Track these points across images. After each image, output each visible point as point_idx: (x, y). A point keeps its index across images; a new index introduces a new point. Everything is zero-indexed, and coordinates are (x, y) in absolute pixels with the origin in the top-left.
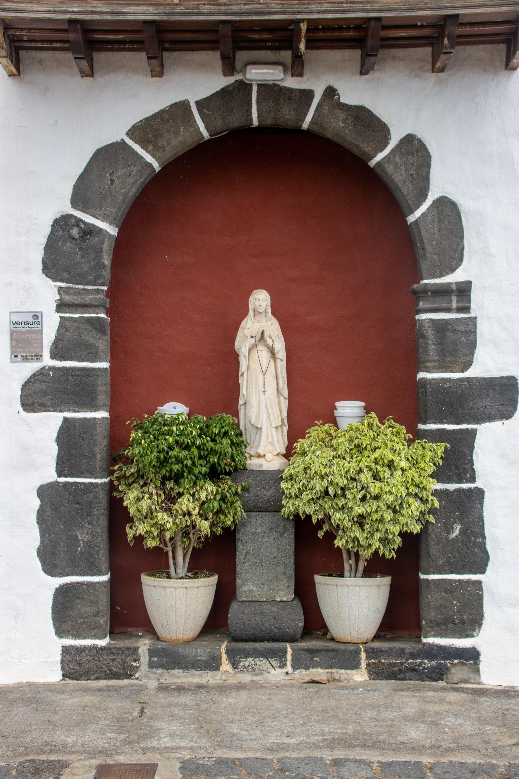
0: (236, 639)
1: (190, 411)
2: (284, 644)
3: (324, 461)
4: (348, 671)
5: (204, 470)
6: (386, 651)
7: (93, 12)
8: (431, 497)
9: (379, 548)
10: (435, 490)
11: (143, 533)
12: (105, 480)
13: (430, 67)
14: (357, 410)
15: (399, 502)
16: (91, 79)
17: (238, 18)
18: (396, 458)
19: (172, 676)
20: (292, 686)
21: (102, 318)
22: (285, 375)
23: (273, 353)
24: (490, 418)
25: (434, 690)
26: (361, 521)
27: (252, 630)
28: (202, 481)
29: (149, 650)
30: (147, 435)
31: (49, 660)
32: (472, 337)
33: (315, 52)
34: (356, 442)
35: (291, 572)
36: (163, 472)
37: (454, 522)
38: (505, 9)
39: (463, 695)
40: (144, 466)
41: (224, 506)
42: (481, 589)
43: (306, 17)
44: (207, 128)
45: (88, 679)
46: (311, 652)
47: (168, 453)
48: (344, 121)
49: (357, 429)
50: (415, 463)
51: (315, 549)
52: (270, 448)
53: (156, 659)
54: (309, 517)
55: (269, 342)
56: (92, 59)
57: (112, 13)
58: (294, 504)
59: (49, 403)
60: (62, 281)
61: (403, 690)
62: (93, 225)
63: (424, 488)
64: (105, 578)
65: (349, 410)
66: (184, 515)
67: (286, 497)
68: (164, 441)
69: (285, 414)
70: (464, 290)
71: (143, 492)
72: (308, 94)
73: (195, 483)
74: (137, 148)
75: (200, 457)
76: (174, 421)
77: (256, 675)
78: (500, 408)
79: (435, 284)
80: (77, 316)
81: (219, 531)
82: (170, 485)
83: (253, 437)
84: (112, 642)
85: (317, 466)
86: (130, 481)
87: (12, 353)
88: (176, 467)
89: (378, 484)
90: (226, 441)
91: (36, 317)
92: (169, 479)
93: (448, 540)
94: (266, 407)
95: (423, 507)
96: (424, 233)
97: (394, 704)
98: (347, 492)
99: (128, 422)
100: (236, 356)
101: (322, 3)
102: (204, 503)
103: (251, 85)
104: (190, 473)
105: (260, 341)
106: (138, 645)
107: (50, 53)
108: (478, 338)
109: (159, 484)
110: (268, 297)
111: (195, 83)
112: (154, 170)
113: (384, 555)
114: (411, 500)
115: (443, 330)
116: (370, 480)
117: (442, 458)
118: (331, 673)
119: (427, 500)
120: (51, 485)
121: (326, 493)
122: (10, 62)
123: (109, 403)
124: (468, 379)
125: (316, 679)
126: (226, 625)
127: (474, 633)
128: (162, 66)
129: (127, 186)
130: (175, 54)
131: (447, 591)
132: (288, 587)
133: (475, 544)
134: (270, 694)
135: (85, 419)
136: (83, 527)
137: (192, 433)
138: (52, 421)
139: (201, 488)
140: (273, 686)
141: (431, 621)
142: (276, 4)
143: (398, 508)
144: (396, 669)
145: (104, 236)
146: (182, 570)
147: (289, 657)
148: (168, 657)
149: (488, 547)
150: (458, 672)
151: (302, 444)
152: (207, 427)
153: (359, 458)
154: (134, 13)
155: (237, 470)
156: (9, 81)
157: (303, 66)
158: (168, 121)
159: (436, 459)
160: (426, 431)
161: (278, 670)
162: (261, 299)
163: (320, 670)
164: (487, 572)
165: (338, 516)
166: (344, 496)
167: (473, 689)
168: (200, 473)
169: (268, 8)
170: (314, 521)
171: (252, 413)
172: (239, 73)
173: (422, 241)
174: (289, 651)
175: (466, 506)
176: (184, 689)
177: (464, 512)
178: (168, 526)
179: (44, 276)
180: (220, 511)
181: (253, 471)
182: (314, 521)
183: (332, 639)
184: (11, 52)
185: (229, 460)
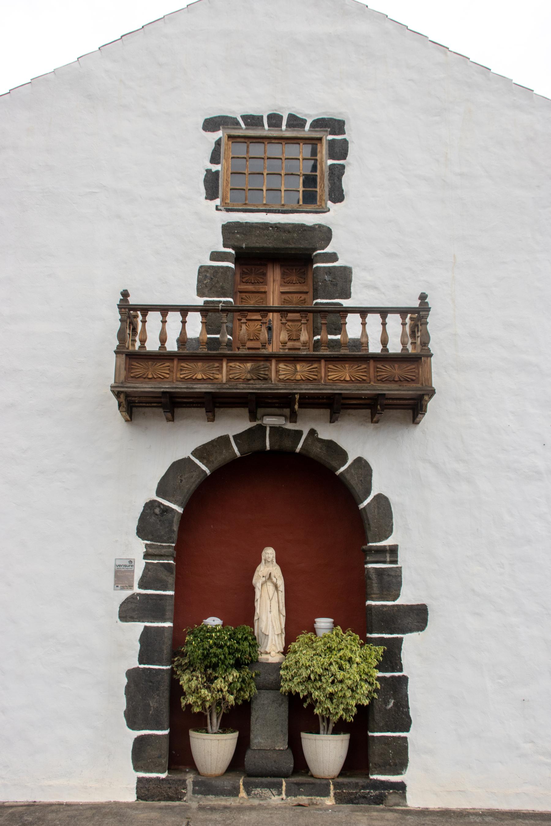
0: (249, 775)
1: (223, 623)
2: (281, 779)
3: (308, 657)
4: (322, 798)
5: (232, 662)
6: (347, 784)
8: (375, 682)
9: (343, 715)
10: (378, 677)
11: (191, 703)
12: (168, 667)
13: (370, 420)
14: (328, 624)
15: (355, 684)
16: (173, 423)
17: (259, 391)
18: (353, 656)
19: (208, 800)
20: (286, 808)
21: (171, 563)
22: (284, 601)
23: (276, 587)
24: (411, 631)
25: (377, 811)
26: (331, 696)
27: (260, 769)
28: (230, 669)
29: (193, 781)
30: (196, 639)
31: (128, 786)
32: (399, 579)
33: (304, 410)
34: (328, 645)
35: (286, 730)
36: (206, 663)
37: (390, 698)
38: (411, 392)
39: (396, 814)
40: (194, 659)
41: (244, 686)
42: (407, 743)
44: (239, 450)
45: (153, 801)
46: (298, 784)
47: (209, 650)
48: (321, 448)
49: (329, 636)
50: (365, 659)
51: (302, 716)
52: (274, 648)
53: (197, 788)
54: (298, 694)
55: (274, 580)
56: (174, 412)
57: (187, 388)
58: (288, 685)
59: (136, 617)
60: (148, 540)
61: (357, 811)
62: (168, 506)
63: (371, 676)
64: (166, 732)
65: (323, 624)
66: (218, 691)
67: (284, 681)
68: (207, 643)
69: (283, 626)
70: (393, 550)
71: (193, 676)
72: (300, 433)
73: (226, 671)
74: (197, 461)
75: (229, 654)
76: (213, 630)
77: (262, 800)
78: (417, 624)
79: (376, 546)
80: (156, 562)
81: (240, 702)
82: (209, 671)
83: (263, 641)
84: (170, 775)
85: (303, 661)
86: (184, 668)
87: (115, 585)
88: (214, 660)
89: (342, 673)
90: (246, 643)
91: (131, 562)
92: (209, 667)
93: (386, 709)
94: (272, 621)
95: (370, 688)
96: (369, 515)
97: (352, 821)
98: (322, 678)
99: (184, 630)
100: (252, 589)
102: (231, 684)
103: (266, 427)
104: (222, 664)
105: (268, 579)
106: (186, 778)
107: (150, 409)
108: (403, 580)
109: (203, 670)
111: (233, 426)
112: (206, 474)
113: (346, 719)
114: (363, 683)
115: (382, 574)
116: (337, 670)
117: (382, 656)
118: (311, 799)
119: (373, 683)
120: (136, 670)
121: (309, 678)
123: (172, 617)
124: (397, 606)
125: (301, 803)
126: (243, 765)
127: (403, 772)
128: (214, 416)
129: (190, 484)
131: (385, 744)
132: (284, 740)
133: (403, 712)
134: (271, 814)
135: (158, 627)
136: (154, 698)
137: (225, 637)
138: (138, 627)
139: (230, 674)
140: (273, 808)
141: (375, 764)
143: (354, 688)
144: (353, 796)
145: (175, 513)
146: (216, 728)
147: (284, 788)
148: (206, 787)
149: (411, 714)
150: (392, 799)
151: (294, 645)
152: (234, 633)
153: (330, 656)
154: (200, 388)
155: (253, 662)
157: (296, 418)
158: (216, 446)
159: (378, 657)
160: (371, 638)
161: (277, 797)
162: (269, 553)
163: (304, 797)
164: (410, 731)
165: (317, 693)
166: (320, 680)
167: (402, 810)
168: (229, 664)
170: (301, 696)
171: (263, 625)
173: (368, 520)
174: (284, 784)
175: (397, 688)
176: (215, 809)
177: (396, 691)
178: (208, 698)
179: (137, 537)
180: (241, 689)
181: (262, 663)
182: (301, 696)
183: (312, 776)
185: (247, 656)
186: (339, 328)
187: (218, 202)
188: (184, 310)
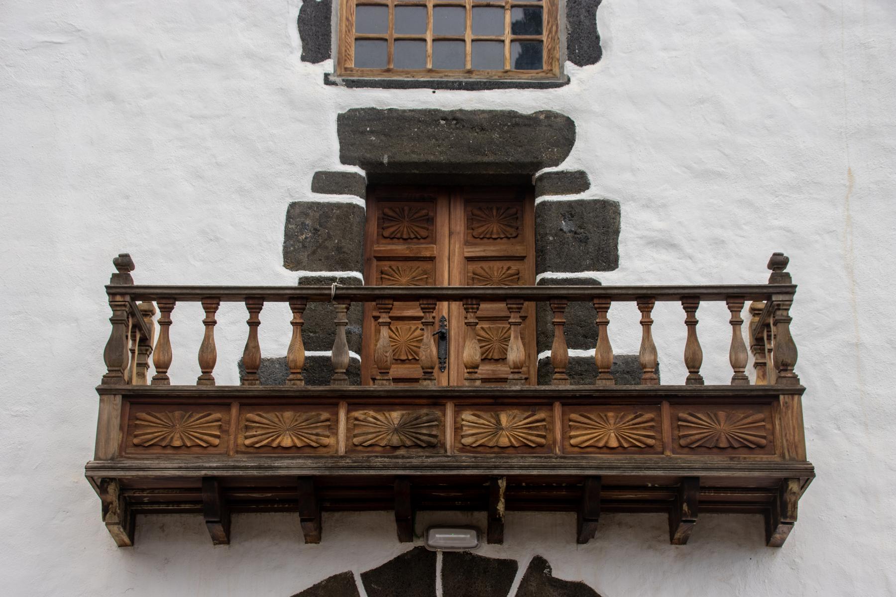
7: (235, 468)
13: (667, 537)
16: (226, 547)
33: (518, 514)
38: (756, 474)
43: (505, 472)
56: (230, 522)
57: (259, 468)
72: (510, 567)
101: (525, 457)
103: (434, 554)
107: (176, 517)
110: (520, 50)
122: (122, 530)
130: (337, 515)
142: (467, 457)
156: (118, 553)
169: (457, 461)
172: (419, 538)
184: (125, 517)
186: (592, 333)
187: (328, 65)
188: (255, 298)
